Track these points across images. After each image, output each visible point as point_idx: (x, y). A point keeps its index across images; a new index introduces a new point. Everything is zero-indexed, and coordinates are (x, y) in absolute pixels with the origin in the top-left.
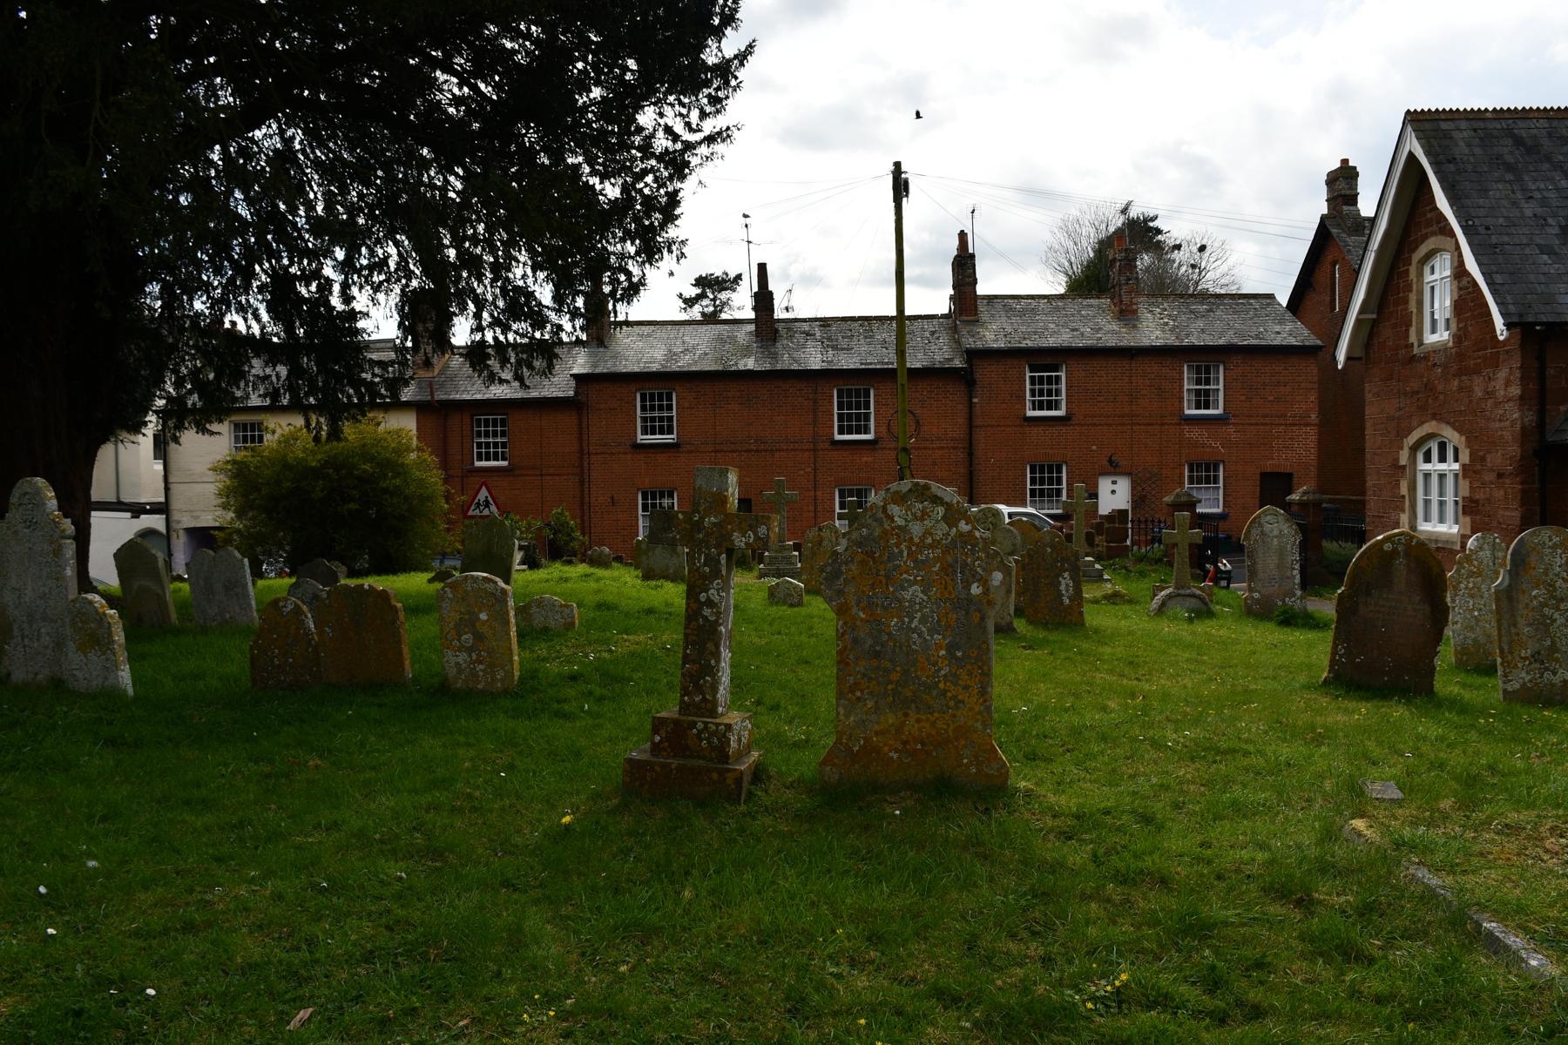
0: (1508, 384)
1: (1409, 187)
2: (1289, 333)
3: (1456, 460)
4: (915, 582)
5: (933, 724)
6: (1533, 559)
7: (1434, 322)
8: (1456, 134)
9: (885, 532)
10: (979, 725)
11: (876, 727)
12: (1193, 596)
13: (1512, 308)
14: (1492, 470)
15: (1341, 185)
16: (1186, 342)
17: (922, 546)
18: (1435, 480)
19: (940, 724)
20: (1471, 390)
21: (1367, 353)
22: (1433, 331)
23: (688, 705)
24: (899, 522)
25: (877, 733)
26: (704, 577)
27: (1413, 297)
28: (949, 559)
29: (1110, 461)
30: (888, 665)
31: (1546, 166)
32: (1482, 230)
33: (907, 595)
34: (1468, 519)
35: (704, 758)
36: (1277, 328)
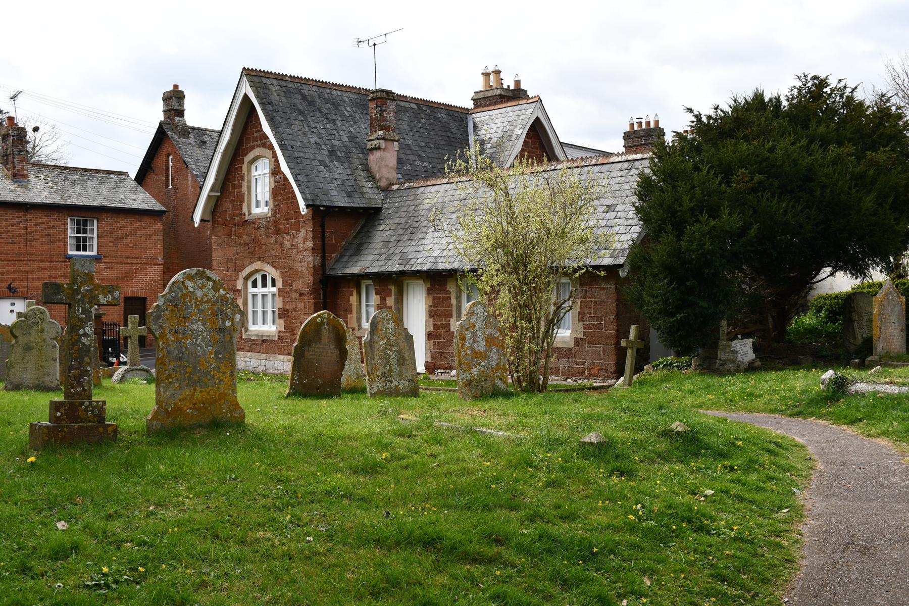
0: (305, 240)
1: (246, 117)
2: (141, 200)
3: (274, 285)
4: (199, 320)
5: (208, 393)
6: (380, 326)
7: (257, 202)
8: (271, 87)
9: (184, 295)
10: (230, 392)
11: (180, 397)
12: (143, 370)
13: (308, 196)
14: (296, 291)
15: (174, 102)
16: (69, 202)
17: (202, 302)
18: (259, 298)
19: (212, 393)
20: (282, 243)
21: (214, 218)
22: (257, 206)
23: (73, 394)
24: (191, 289)
25: (180, 400)
26: (82, 320)
27: (245, 184)
28: (215, 308)
29: (10, 288)
30: (186, 364)
31: (319, 114)
32: (289, 148)
33: (195, 327)
34: (282, 321)
35: (90, 421)
36: (134, 197)
